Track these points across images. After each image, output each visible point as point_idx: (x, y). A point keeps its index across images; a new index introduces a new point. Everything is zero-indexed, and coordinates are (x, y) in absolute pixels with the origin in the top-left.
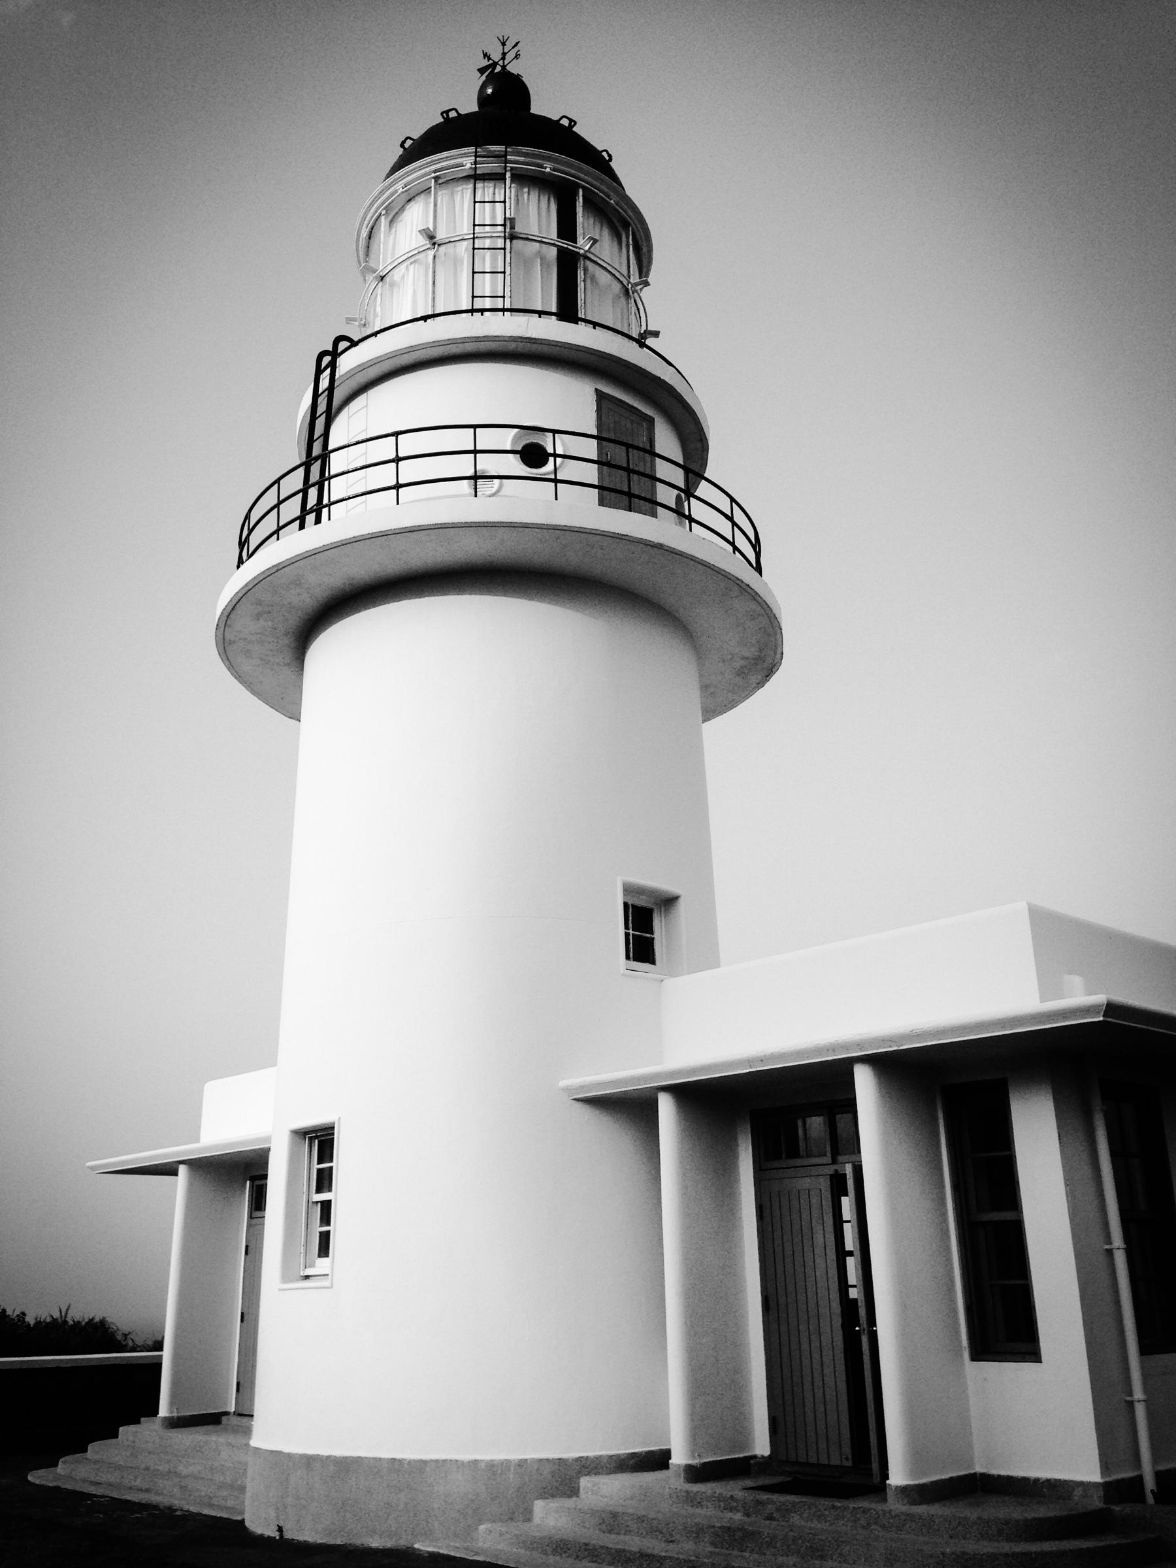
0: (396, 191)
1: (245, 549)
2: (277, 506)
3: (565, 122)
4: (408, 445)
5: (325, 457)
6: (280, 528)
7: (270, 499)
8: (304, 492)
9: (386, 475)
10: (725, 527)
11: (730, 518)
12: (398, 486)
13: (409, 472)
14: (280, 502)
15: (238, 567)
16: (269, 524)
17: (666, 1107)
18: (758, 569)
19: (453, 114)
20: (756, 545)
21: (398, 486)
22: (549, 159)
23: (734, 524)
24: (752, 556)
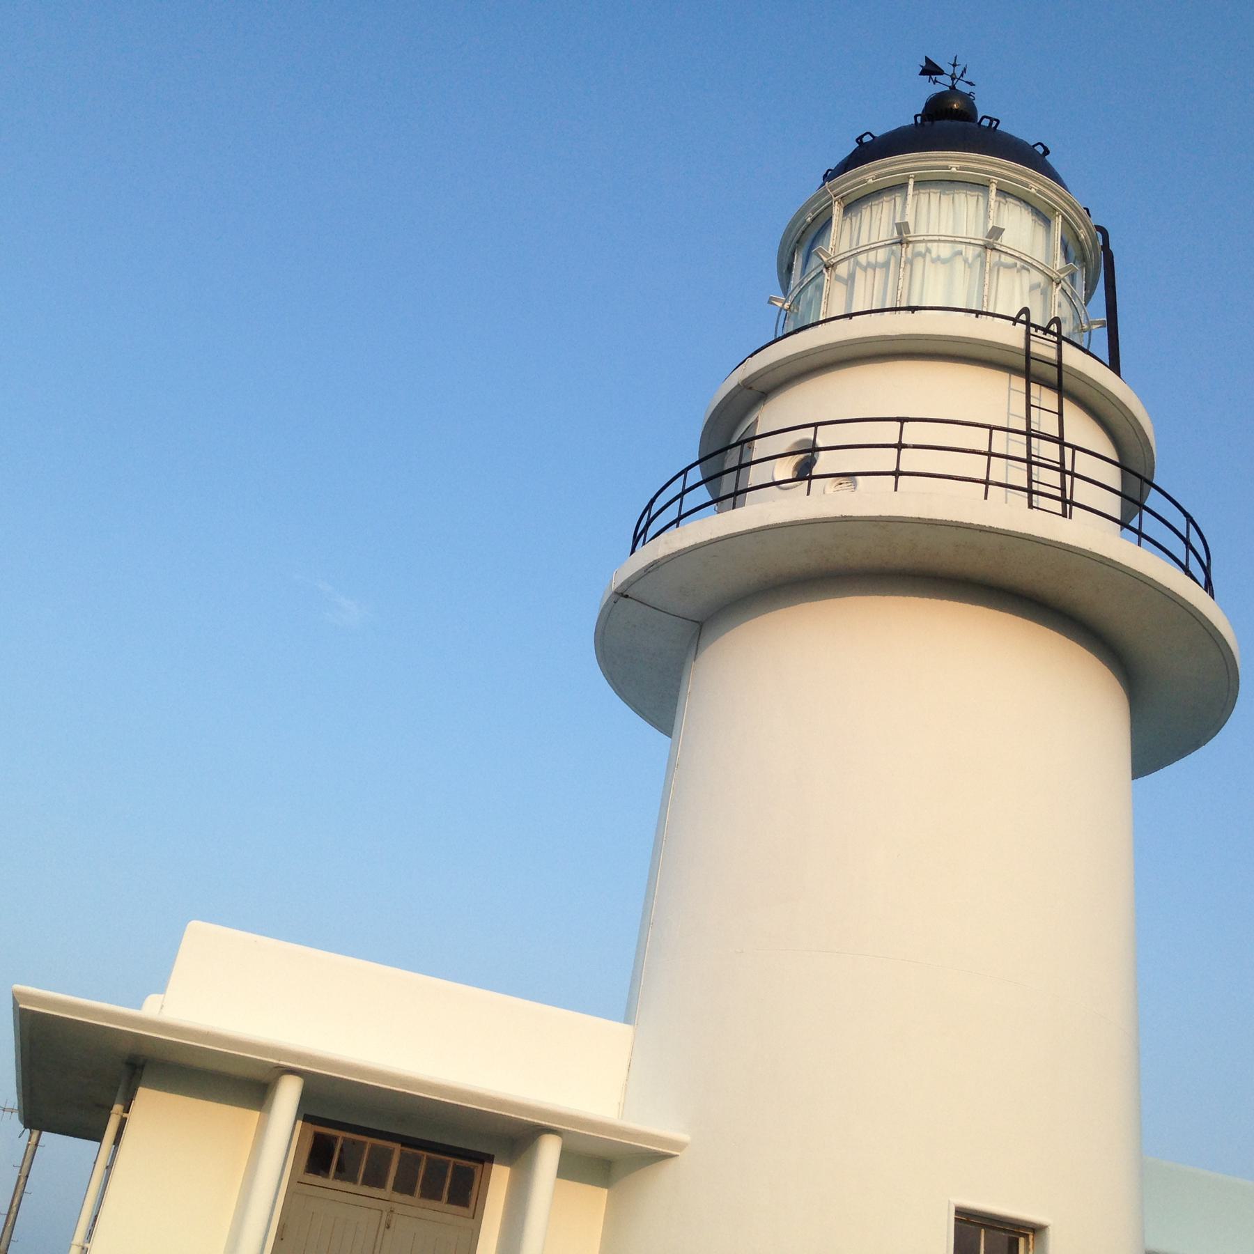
0: (947, 168)
1: (638, 537)
2: (681, 496)
3: (1040, 149)
4: (913, 433)
5: (1059, 388)
6: (681, 517)
7: (676, 488)
8: (1060, 441)
9: (886, 460)
10: (1179, 549)
11: (1186, 541)
12: (897, 473)
13: (910, 460)
14: (685, 492)
15: (633, 551)
16: (672, 513)
17: (288, 1095)
18: (1208, 587)
19: (867, 139)
20: (1207, 570)
21: (897, 473)
22: (1036, 180)
23: (1189, 546)
24: (1201, 577)
